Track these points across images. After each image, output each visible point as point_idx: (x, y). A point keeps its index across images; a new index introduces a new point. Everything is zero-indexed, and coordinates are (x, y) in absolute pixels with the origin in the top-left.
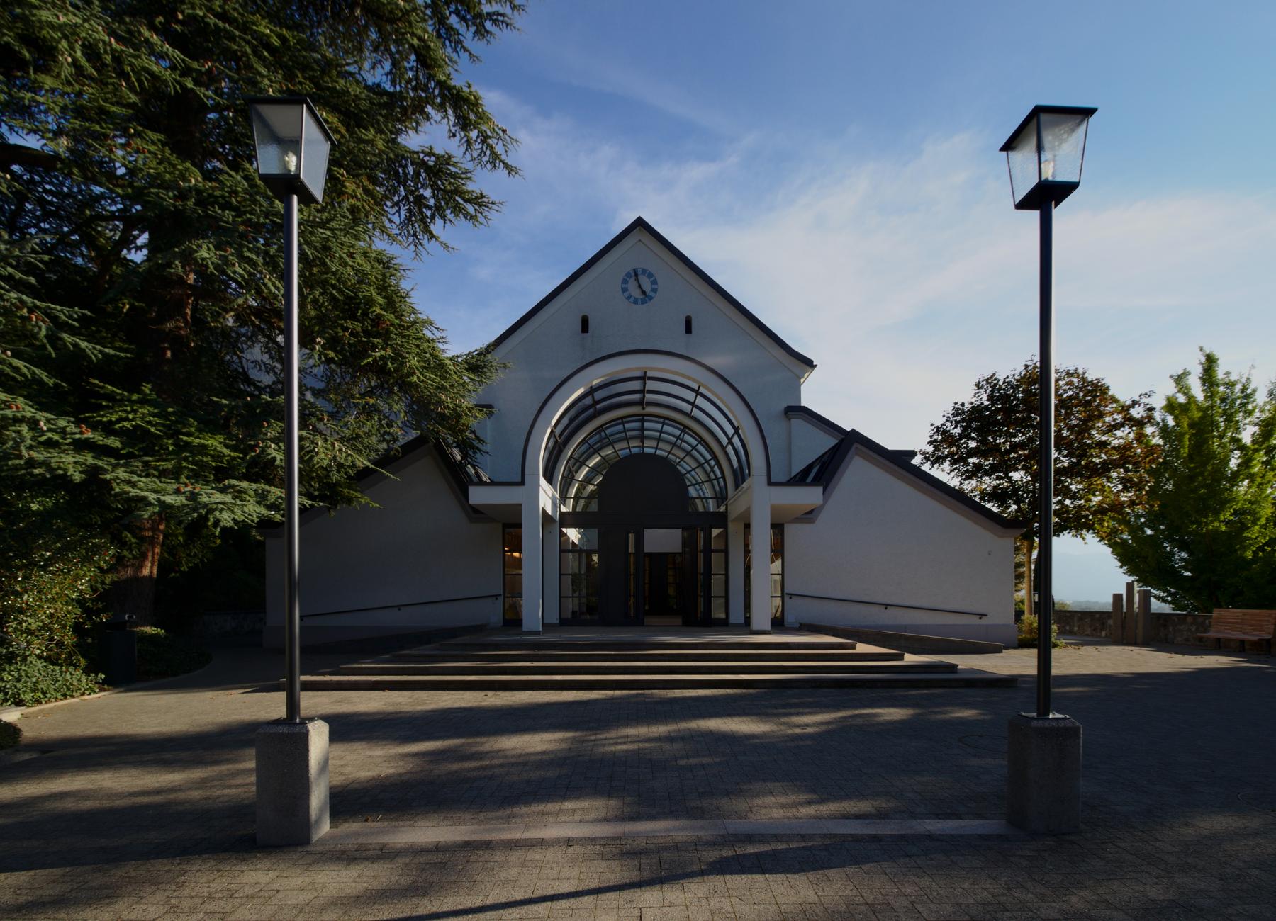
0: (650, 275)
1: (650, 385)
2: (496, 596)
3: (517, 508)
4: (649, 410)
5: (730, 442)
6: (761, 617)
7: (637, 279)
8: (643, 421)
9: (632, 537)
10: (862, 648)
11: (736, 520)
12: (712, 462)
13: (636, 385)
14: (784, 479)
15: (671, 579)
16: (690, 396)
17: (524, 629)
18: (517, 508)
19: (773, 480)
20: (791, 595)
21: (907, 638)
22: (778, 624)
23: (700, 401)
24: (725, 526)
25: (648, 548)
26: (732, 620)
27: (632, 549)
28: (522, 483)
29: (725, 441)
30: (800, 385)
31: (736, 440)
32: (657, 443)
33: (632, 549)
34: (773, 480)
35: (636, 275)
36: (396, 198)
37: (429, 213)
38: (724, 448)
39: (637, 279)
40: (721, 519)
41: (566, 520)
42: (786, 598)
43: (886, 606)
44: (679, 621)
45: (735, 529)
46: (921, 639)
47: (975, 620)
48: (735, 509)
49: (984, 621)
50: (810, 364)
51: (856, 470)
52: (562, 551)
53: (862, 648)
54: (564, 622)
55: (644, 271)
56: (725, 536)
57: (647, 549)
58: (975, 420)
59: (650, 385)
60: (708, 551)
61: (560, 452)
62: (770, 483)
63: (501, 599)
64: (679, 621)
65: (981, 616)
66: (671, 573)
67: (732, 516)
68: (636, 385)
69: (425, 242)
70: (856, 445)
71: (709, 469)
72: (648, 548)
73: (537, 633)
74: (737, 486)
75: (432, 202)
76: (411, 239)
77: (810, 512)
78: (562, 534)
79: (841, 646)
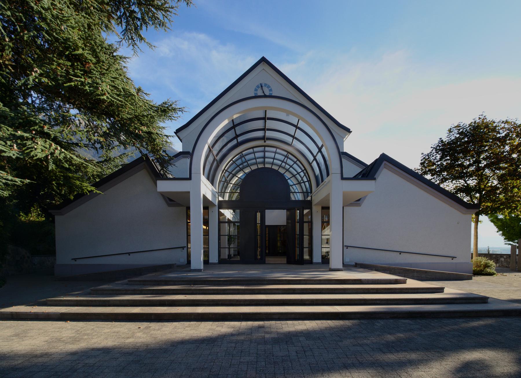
0: (269, 87)
1: (270, 124)
2: (183, 248)
3: (186, 195)
4: (268, 142)
5: (315, 159)
6: (336, 261)
7: (262, 89)
8: (264, 151)
9: (259, 215)
10: (411, 283)
11: (317, 204)
12: (302, 174)
13: (259, 124)
14: (352, 176)
15: (278, 238)
16: (291, 130)
17: (192, 268)
18: (186, 195)
19: (344, 176)
20: (347, 247)
21: (418, 271)
22: (347, 267)
23: (299, 134)
24: (310, 208)
25: (268, 223)
26: (315, 260)
27: (258, 221)
28: (190, 179)
29: (311, 158)
30: (343, 142)
31: (319, 157)
32: (274, 158)
33: (258, 221)
34: (344, 176)
35: (262, 87)
36: (118, 14)
37: (139, 23)
38: (310, 164)
39: (262, 89)
40: (307, 204)
41: (221, 205)
42: (345, 248)
43: (400, 252)
44: (284, 260)
45: (317, 211)
46: (426, 272)
47: (449, 260)
48: (317, 197)
49: (455, 261)
50: (348, 131)
51: (385, 174)
52: (220, 222)
53: (411, 283)
54: (222, 261)
55: (266, 85)
56: (311, 213)
57: (267, 223)
58: (447, 149)
59: (270, 124)
60: (302, 222)
61: (218, 166)
62: (343, 178)
63: (186, 249)
64: (284, 260)
65: (453, 258)
66: (279, 235)
67: (314, 203)
68: (259, 124)
69: (138, 43)
70: (385, 162)
71: (300, 179)
72: (268, 223)
73: (200, 270)
74: (318, 185)
75: (139, 16)
76: (130, 41)
77: (359, 200)
78: (220, 214)
79: (396, 282)
